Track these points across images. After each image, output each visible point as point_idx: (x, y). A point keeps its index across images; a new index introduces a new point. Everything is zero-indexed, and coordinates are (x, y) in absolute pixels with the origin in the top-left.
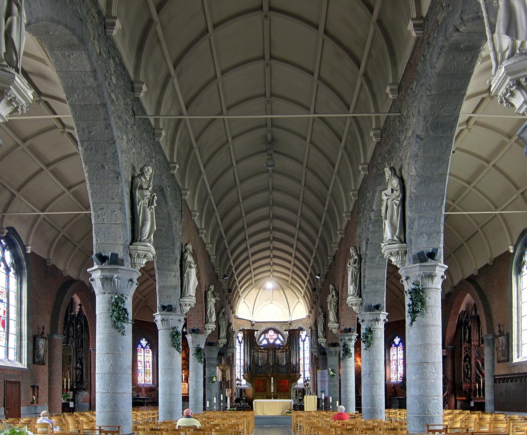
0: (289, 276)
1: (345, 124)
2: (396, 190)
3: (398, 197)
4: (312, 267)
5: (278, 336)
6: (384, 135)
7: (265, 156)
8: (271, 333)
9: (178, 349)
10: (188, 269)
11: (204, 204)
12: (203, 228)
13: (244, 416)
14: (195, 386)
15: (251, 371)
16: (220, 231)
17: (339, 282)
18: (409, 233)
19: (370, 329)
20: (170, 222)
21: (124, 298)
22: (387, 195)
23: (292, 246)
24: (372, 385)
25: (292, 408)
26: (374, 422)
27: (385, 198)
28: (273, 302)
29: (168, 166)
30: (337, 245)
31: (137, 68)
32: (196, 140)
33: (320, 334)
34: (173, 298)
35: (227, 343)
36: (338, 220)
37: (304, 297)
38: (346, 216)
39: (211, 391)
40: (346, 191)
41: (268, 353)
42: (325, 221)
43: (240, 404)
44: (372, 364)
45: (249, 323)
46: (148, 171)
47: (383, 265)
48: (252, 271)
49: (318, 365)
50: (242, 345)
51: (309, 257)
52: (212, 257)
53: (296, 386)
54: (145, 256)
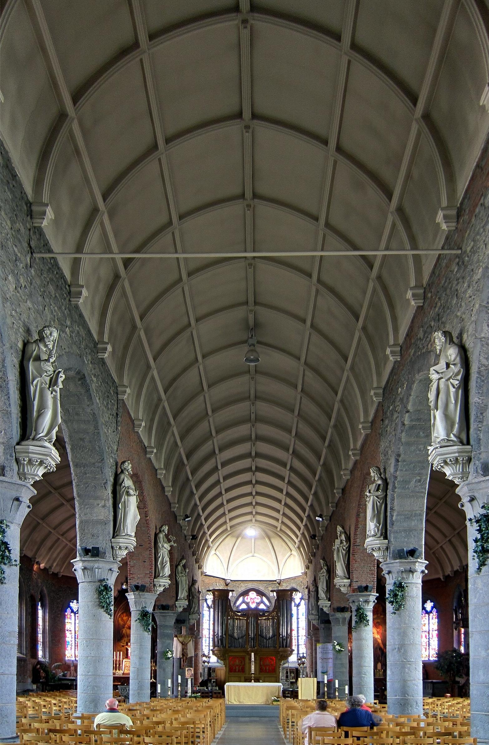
0: (277, 520)
1: (364, 293)
2: (454, 364)
3: (457, 374)
4: (312, 506)
5: (262, 599)
6: (429, 295)
7: (245, 348)
8: (253, 595)
9: (107, 611)
10: (124, 498)
11: (154, 413)
12: (153, 445)
13: (209, 707)
14: (136, 663)
15: (225, 645)
16: (180, 453)
17: (351, 523)
18: (475, 429)
19: (401, 583)
20: (96, 427)
21: (4, 526)
22: (438, 373)
23: (282, 478)
24: (404, 664)
25: (281, 694)
26: (409, 720)
27: (434, 377)
28: (255, 555)
29: (95, 347)
30: (348, 472)
31: (38, 183)
32: (142, 318)
33: (322, 594)
34: (101, 538)
35: (190, 606)
36: (351, 436)
37: (299, 548)
38: (363, 427)
39: (164, 670)
40: (363, 393)
41: (247, 620)
42: (331, 441)
43: (207, 688)
44: (404, 634)
45: (222, 583)
46: (51, 334)
47: (422, 492)
48: (227, 512)
49: (317, 637)
50: (212, 610)
51: (306, 494)
52: (166, 489)
53: (286, 665)
54: (41, 463)
